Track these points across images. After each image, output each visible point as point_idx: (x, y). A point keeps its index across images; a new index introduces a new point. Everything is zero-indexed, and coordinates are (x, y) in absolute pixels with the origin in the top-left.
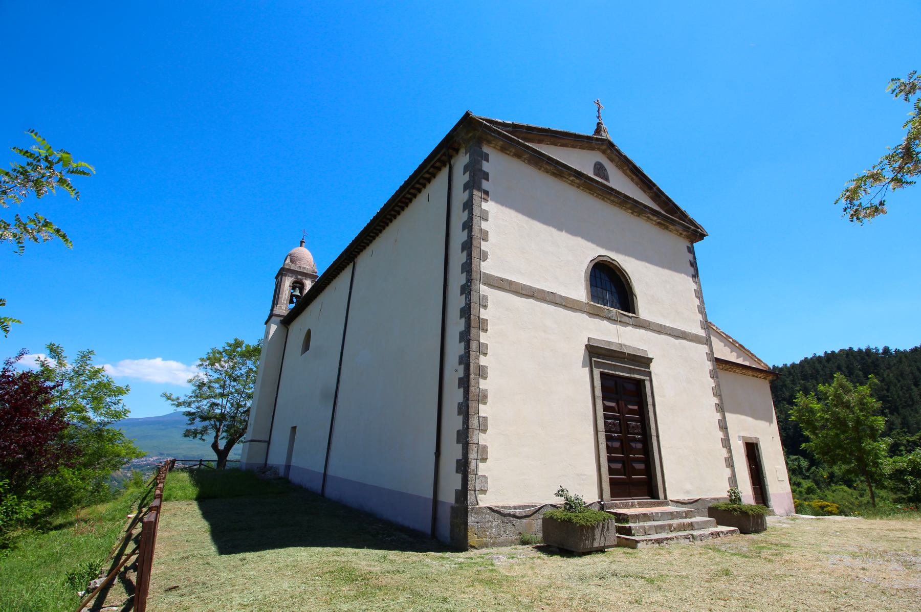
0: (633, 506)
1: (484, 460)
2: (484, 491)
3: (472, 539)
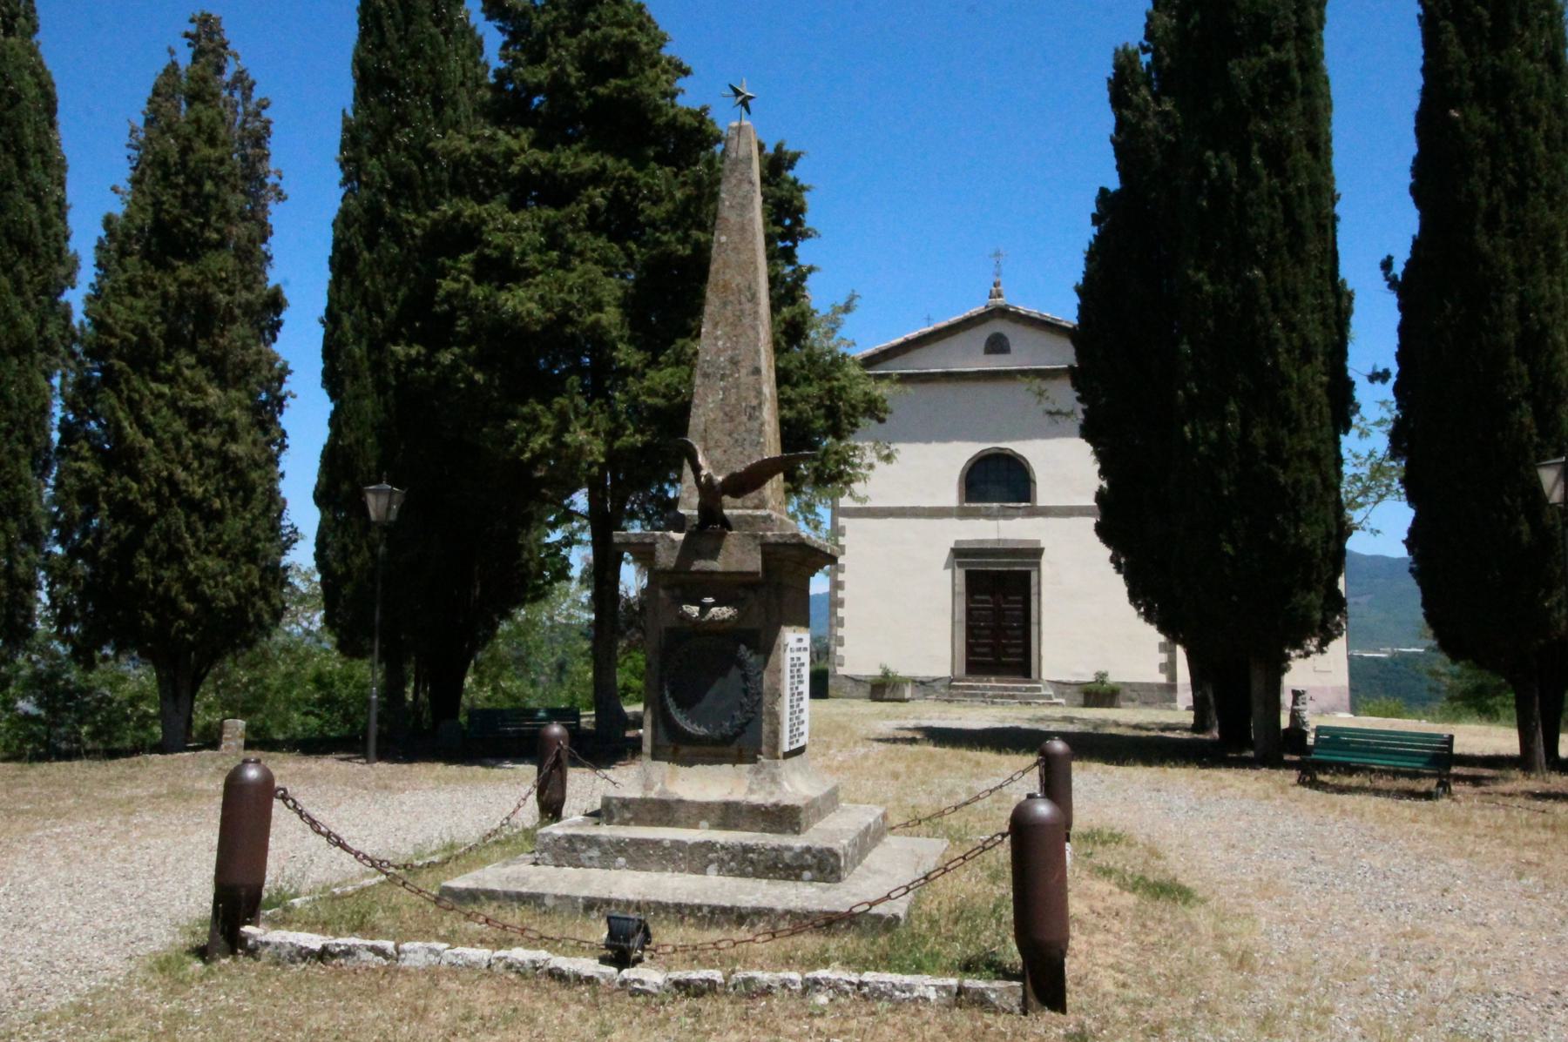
0: (988, 681)
1: (842, 645)
2: (841, 665)
3: (831, 692)
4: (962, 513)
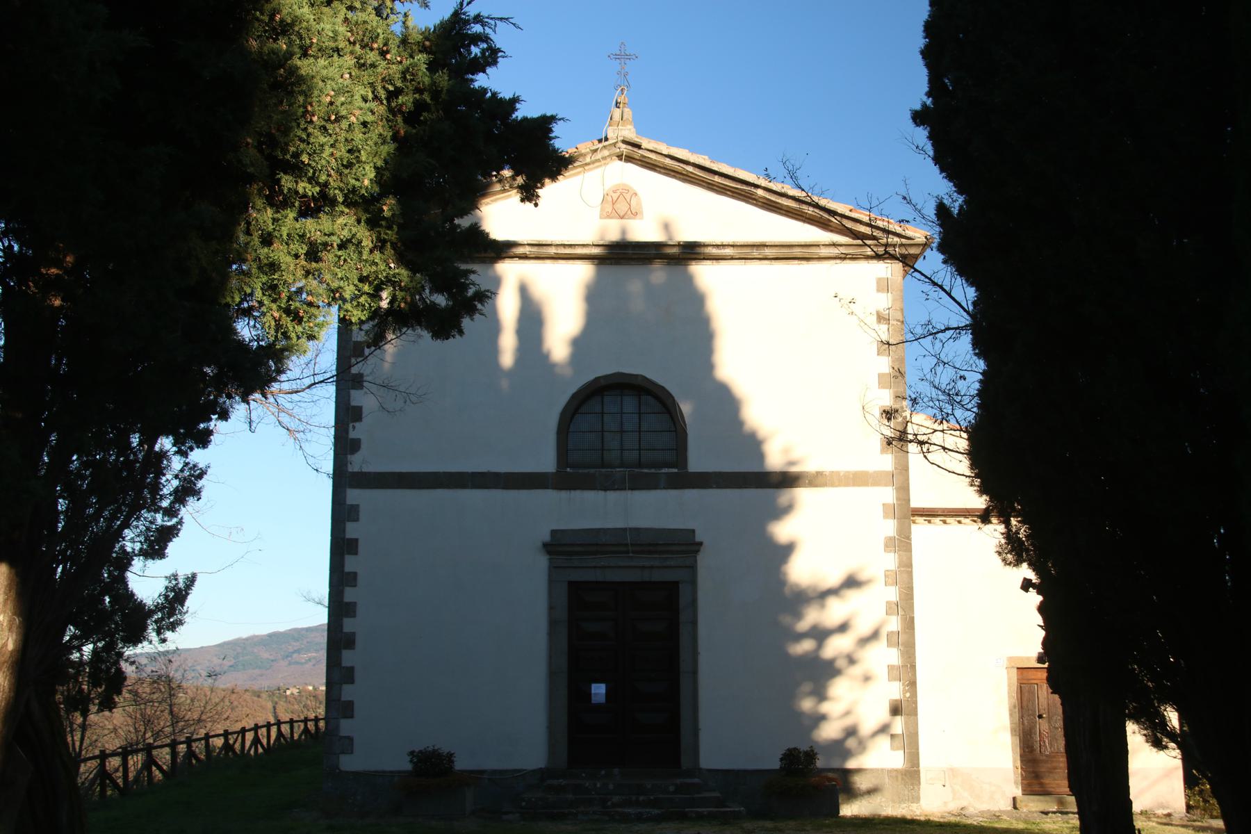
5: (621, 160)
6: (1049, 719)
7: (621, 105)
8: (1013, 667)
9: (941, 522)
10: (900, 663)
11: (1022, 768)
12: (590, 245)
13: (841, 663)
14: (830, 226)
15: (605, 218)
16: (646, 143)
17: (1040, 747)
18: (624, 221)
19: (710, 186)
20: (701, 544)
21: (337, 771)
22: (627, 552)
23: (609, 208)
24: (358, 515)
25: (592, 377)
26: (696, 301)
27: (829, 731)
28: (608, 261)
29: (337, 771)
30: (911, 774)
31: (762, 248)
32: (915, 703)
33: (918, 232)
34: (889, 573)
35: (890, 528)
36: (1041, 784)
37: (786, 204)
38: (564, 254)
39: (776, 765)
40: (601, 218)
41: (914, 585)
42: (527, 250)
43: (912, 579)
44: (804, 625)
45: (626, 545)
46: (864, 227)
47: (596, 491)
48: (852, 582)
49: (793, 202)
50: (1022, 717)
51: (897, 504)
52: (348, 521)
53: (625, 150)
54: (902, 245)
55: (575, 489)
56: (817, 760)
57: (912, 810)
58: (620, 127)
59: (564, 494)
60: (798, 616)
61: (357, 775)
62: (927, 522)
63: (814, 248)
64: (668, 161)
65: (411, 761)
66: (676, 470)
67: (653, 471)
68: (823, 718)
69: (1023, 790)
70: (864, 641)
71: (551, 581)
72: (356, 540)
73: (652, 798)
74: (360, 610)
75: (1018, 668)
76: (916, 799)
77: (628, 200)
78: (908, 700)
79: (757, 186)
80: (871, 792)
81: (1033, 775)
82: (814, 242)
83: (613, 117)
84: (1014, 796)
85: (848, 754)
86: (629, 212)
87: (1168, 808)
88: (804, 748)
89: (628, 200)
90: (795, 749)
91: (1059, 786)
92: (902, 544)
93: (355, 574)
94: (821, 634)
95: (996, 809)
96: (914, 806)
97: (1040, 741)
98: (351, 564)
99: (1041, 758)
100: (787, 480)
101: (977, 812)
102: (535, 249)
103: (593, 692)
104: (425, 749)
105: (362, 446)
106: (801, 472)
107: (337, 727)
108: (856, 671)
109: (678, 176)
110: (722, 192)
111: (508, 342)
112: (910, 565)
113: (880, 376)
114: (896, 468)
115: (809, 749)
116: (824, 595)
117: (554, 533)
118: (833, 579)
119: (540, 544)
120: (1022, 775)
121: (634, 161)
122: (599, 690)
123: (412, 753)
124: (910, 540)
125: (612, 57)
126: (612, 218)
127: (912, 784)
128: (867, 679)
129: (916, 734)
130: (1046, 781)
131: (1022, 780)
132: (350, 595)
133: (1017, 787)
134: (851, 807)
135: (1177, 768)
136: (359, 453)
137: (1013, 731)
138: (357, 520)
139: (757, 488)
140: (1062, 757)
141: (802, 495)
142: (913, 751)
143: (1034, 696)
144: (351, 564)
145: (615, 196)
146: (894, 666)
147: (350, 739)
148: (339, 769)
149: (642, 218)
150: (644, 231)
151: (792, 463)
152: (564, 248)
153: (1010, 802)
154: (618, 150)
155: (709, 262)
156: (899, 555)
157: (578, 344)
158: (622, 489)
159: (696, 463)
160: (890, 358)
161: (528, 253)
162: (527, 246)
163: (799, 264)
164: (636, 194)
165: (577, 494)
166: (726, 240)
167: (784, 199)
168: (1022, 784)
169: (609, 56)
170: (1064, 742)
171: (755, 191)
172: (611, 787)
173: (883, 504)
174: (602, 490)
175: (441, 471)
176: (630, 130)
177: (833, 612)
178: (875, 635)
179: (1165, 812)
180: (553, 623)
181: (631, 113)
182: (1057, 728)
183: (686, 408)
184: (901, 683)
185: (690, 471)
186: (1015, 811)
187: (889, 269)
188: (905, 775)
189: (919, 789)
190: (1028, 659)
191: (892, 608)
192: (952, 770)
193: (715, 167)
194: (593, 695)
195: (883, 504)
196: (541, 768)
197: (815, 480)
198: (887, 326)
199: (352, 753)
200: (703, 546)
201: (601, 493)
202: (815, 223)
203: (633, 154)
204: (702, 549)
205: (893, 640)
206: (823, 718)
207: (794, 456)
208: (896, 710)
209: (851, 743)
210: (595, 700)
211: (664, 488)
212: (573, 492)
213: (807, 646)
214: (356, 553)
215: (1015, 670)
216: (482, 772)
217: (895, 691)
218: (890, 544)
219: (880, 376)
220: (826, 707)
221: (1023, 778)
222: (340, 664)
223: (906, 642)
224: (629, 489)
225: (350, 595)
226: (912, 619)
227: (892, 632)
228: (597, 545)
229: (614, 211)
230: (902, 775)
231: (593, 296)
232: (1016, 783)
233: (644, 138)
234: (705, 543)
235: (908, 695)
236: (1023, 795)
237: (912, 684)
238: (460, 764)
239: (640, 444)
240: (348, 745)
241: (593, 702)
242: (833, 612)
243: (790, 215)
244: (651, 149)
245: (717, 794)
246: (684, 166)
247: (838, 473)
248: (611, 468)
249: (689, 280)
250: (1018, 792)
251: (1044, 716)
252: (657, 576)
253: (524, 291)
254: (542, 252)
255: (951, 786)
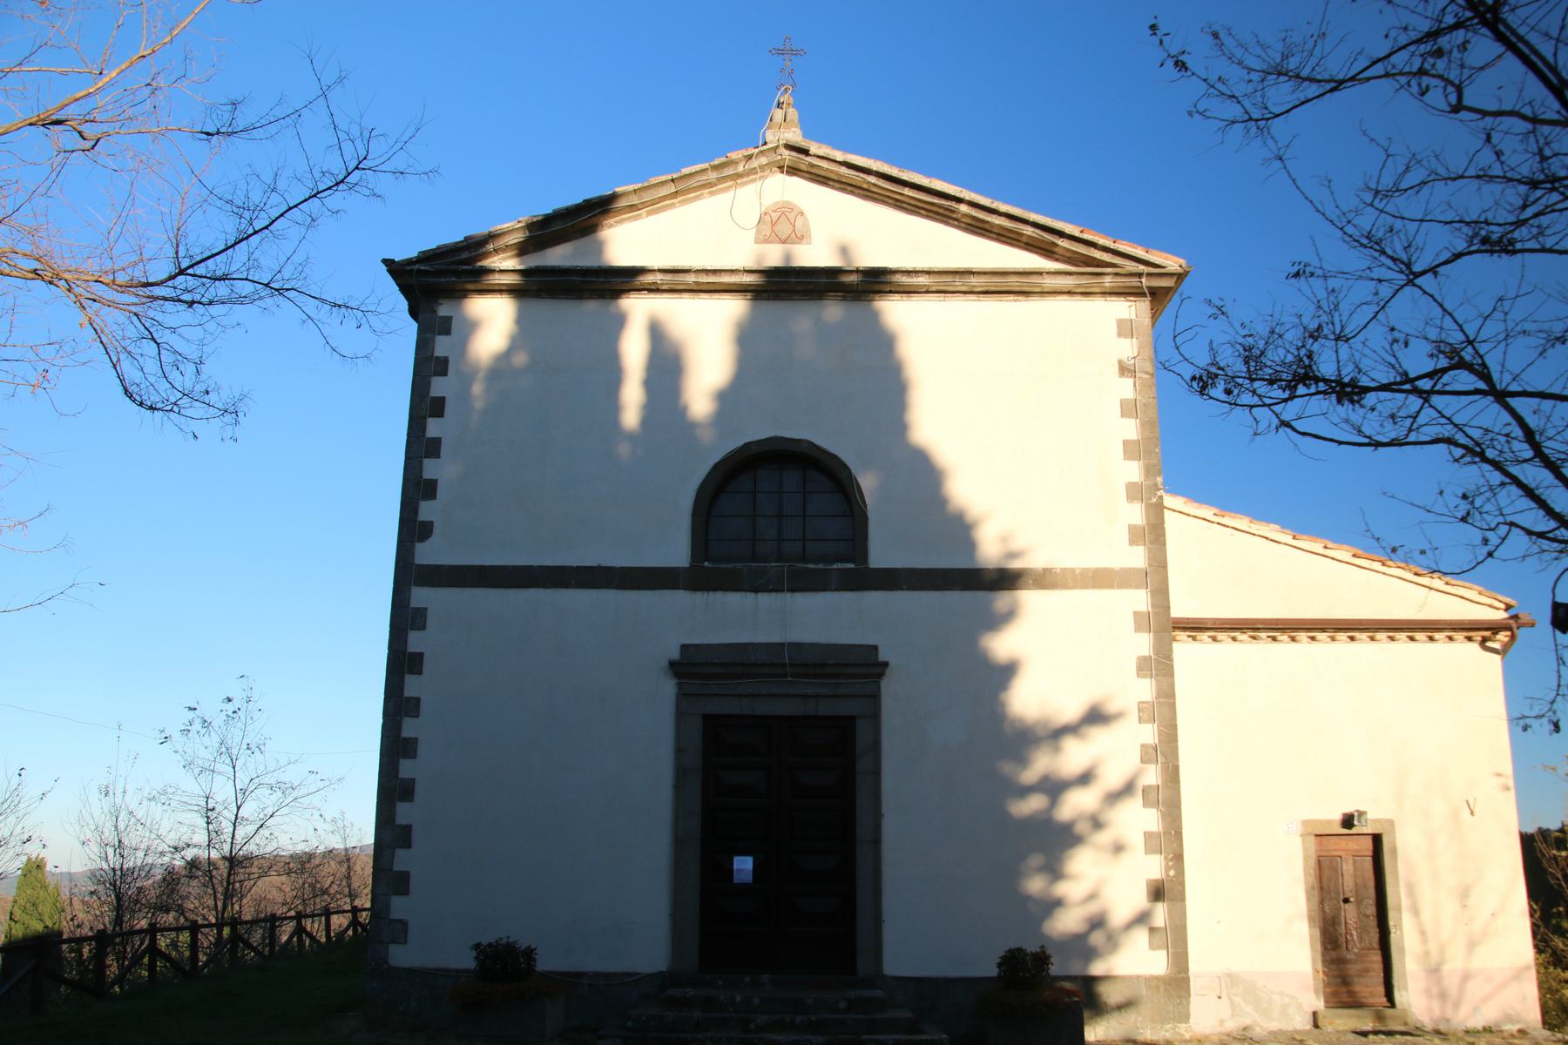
4: (697, 577)
5: (783, 172)
6: (1359, 902)
7: (784, 106)
8: (1310, 834)
9: (1210, 639)
10: (1161, 829)
11: (1324, 972)
12: (740, 271)
13: (1082, 828)
14: (1054, 253)
15: (762, 243)
16: (814, 148)
17: (1347, 942)
18: (786, 246)
19: (898, 203)
20: (886, 664)
21: (386, 966)
22: (785, 675)
23: (767, 231)
24: (425, 622)
25: (740, 443)
26: (884, 343)
27: (1067, 922)
28: (765, 295)
29: (386, 966)
30: (1177, 982)
31: (966, 276)
32: (1182, 884)
33: (1170, 260)
34: (1144, 705)
35: (1144, 644)
36: (1351, 993)
37: (997, 222)
38: (706, 284)
39: (993, 972)
40: (756, 242)
41: (1178, 722)
42: (658, 278)
43: (1175, 713)
44: (1030, 775)
45: (784, 665)
46: (1100, 253)
47: (743, 593)
48: (1096, 717)
49: (1007, 220)
50: (1322, 902)
51: (1153, 612)
52: (411, 629)
53: (788, 157)
54: (1149, 275)
55: (715, 590)
56: (1050, 966)
57: (1178, 1033)
58: (782, 130)
59: (699, 597)
60: (1023, 761)
61: (411, 972)
62: (1190, 639)
63: (1035, 276)
64: (843, 170)
65: (476, 958)
66: (852, 566)
67: (821, 566)
68: (1057, 903)
69: (1326, 1002)
70: (1116, 796)
71: (680, 715)
72: (421, 655)
73: (813, 1018)
74: (422, 749)
75: (1316, 835)
76: (1185, 1017)
77: (792, 221)
78: (1172, 881)
79: (959, 200)
80: (1124, 1006)
81: (1339, 980)
82: (1035, 269)
83: (773, 117)
84: (1314, 1010)
85: (1091, 954)
86: (793, 235)
87: (1518, 1022)
88: (1032, 947)
89: (792, 221)
90: (1019, 950)
91: (1372, 995)
92: (1159, 666)
93: (418, 700)
94: (1055, 788)
95: (1290, 1028)
96: (1182, 1028)
97: (1347, 933)
98: (412, 685)
99: (1348, 957)
100: (1006, 579)
101: (1265, 1033)
102: (669, 277)
103: (735, 867)
104: (496, 941)
105: (435, 531)
106: (1022, 569)
107: (387, 907)
108: (1104, 838)
109: (857, 191)
110: (914, 211)
111: (632, 396)
112: (1171, 695)
113: (1126, 443)
114: (1150, 565)
115: (1038, 950)
116: (1060, 733)
117: (685, 648)
118: (1070, 711)
119: (665, 663)
120: (1323, 980)
121: (799, 173)
122: (744, 865)
123: (477, 946)
124: (1172, 660)
125: (774, 52)
126: (770, 242)
127: (1179, 997)
128: (1118, 848)
129: (1184, 927)
130: (1357, 988)
131: (1324, 987)
132: (409, 728)
133: (1318, 998)
134: (1094, 1029)
135: (1527, 968)
136: (430, 539)
137: (1311, 919)
138: (423, 627)
139: (963, 590)
140: (1376, 955)
141: (1029, 599)
142: (1179, 950)
143: (1338, 873)
144: (412, 685)
145: (775, 216)
146: (1152, 833)
147: (404, 924)
148: (388, 964)
149: (810, 243)
150: (815, 255)
151: (1013, 555)
152: (706, 274)
153: (1309, 1018)
154: (780, 157)
155: (897, 297)
156: (1157, 681)
157: (726, 398)
158: (777, 591)
159: (880, 555)
160: (1138, 420)
161: (659, 282)
162: (658, 274)
163: (1015, 301)
164: (802, 214)
165: (717, 597)
166: (920, 265)
167: (994, 216)
168: (1324, 992)
169: (770, 51)
170: (1378, 935)
171: (956, 206)
172: (756, 1001)
173: (1135, 613)
174: (751, 591)
175: (536, 564)
176: (795, 132)
177: (1073, 756)
178: (1127, 790)
179: (1518, 1026)
180: (681, 773)
181: (796, 113)
182: (1368, 916)
183: (868, 482)
184: (1163, 856)
185: (872, 566)
186: (1317, 1031)
187: (1133, 308)
188: (1169, 984)
189: (1189, 1003)
190: (1330, 822)
191: (1148, 754)
192: (1229, 975)
193: (905, 176)
194: (735, 873)
195: (1135, 613)
196: (662, 972)
197: (1045, 580)
198: (1131, 381)
199: (405, 942)
200: (889, 668)
201: (750, 596)
202: (1036, 250)
203: (799, 164)
204: (887, 671)
205: (1150, 797)
206: (1057, 903)
207: (1016, 545)
208: (1158, 892)
209: (1097, 938)
210: (737, 879)
211: (836, 590)
212: (711, 593)
213: (1034, 804)
214: (420, 673)
215: (1313, 838)
216: (579, 975)
217: (1154, 867)
218: (1144, 667)
219: (1126, 443)
220: (1064, 889)
221: (1326, 985)
222: (394, 820)
223: (1168, 800)
224: (787, 591)
225: (409, 728)
226: (1176, 769)
227: (1150, 787)
228: (742, 664)
229: (773, 234)
230: (1165, 984)
231: (746, 338)
232: (1316, 992)
233: (812, 142)
234: (892, 664)
235: (1172, 873)
236: (1326, 1007)
237: (1178, 858)
238: (545, 963)
239: (804, 533)
240: (400, 931)
241: (735, 882)
242: (1073, 756)
243: (1003, 239)
244: (822, 154)
245: (906, 1014)
246: (865, 176)
247: (1073, 570)
248: (764, 563)
249: (875, 316)
250: (1319, 1004)
251: (1352, 899)
252: (826, 708)
253: (656, 333)
254: (678, 282)
255: (1230, 999)
